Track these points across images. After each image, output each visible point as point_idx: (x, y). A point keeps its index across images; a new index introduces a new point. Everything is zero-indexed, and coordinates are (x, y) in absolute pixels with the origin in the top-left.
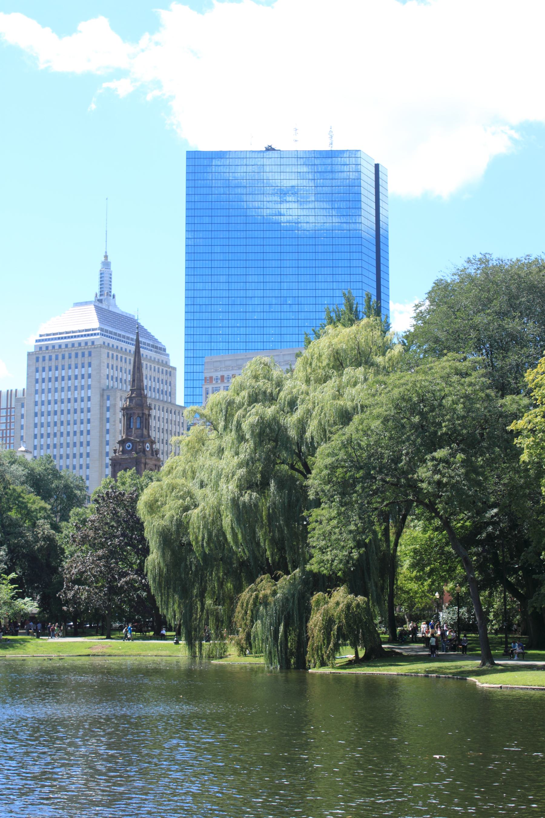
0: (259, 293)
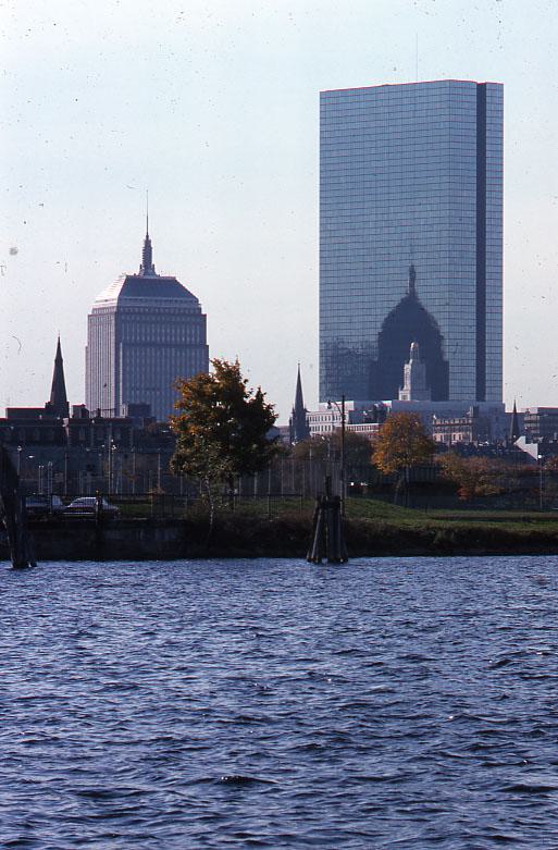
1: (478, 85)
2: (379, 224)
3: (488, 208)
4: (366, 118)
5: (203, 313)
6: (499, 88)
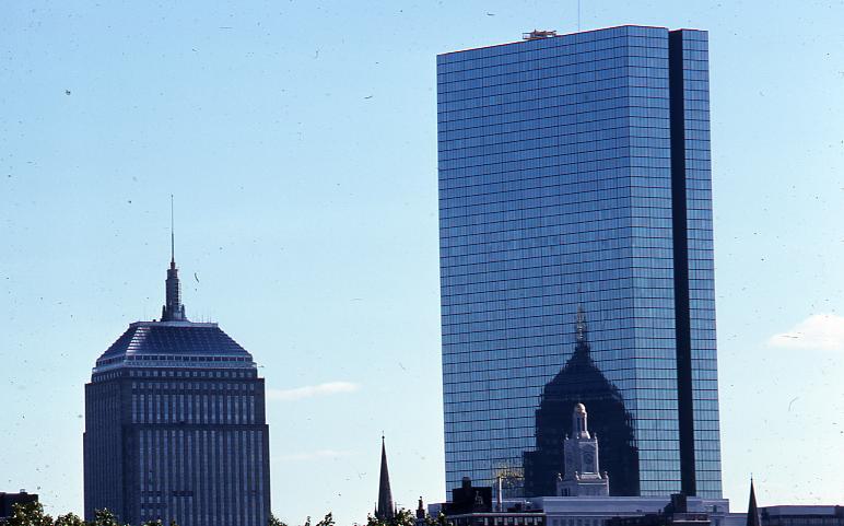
1: (670, 33)
2: (526, 244)
3: (689, 214)
4: (504, 89)
5: (259, 377)
6: (702, 37)
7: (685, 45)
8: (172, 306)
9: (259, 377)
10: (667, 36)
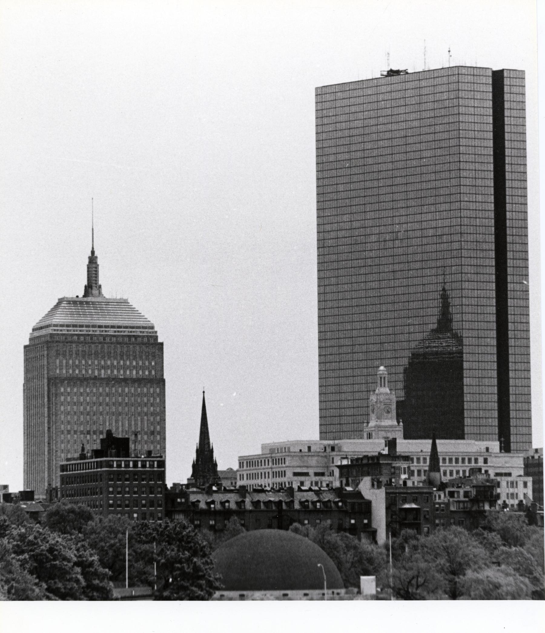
0: (376, 230)
5: (160, 340)
6: (520, 75)
7: (506, 82)
8: (92, 284)
9: (160, 340)
10: (491, 74)
